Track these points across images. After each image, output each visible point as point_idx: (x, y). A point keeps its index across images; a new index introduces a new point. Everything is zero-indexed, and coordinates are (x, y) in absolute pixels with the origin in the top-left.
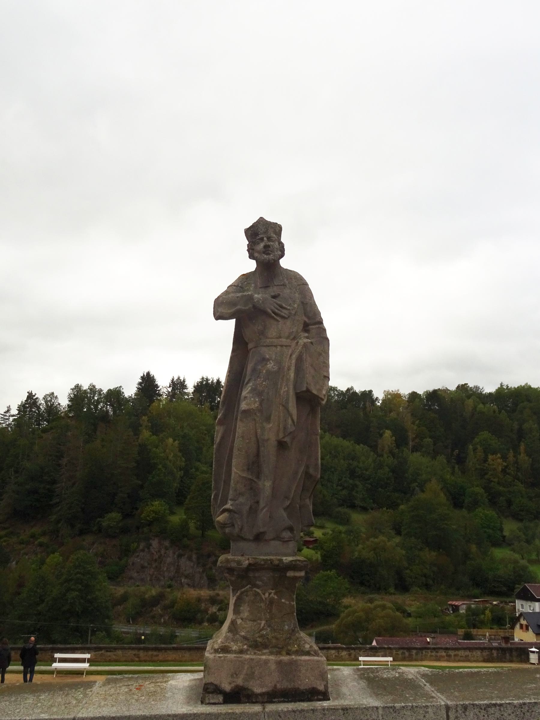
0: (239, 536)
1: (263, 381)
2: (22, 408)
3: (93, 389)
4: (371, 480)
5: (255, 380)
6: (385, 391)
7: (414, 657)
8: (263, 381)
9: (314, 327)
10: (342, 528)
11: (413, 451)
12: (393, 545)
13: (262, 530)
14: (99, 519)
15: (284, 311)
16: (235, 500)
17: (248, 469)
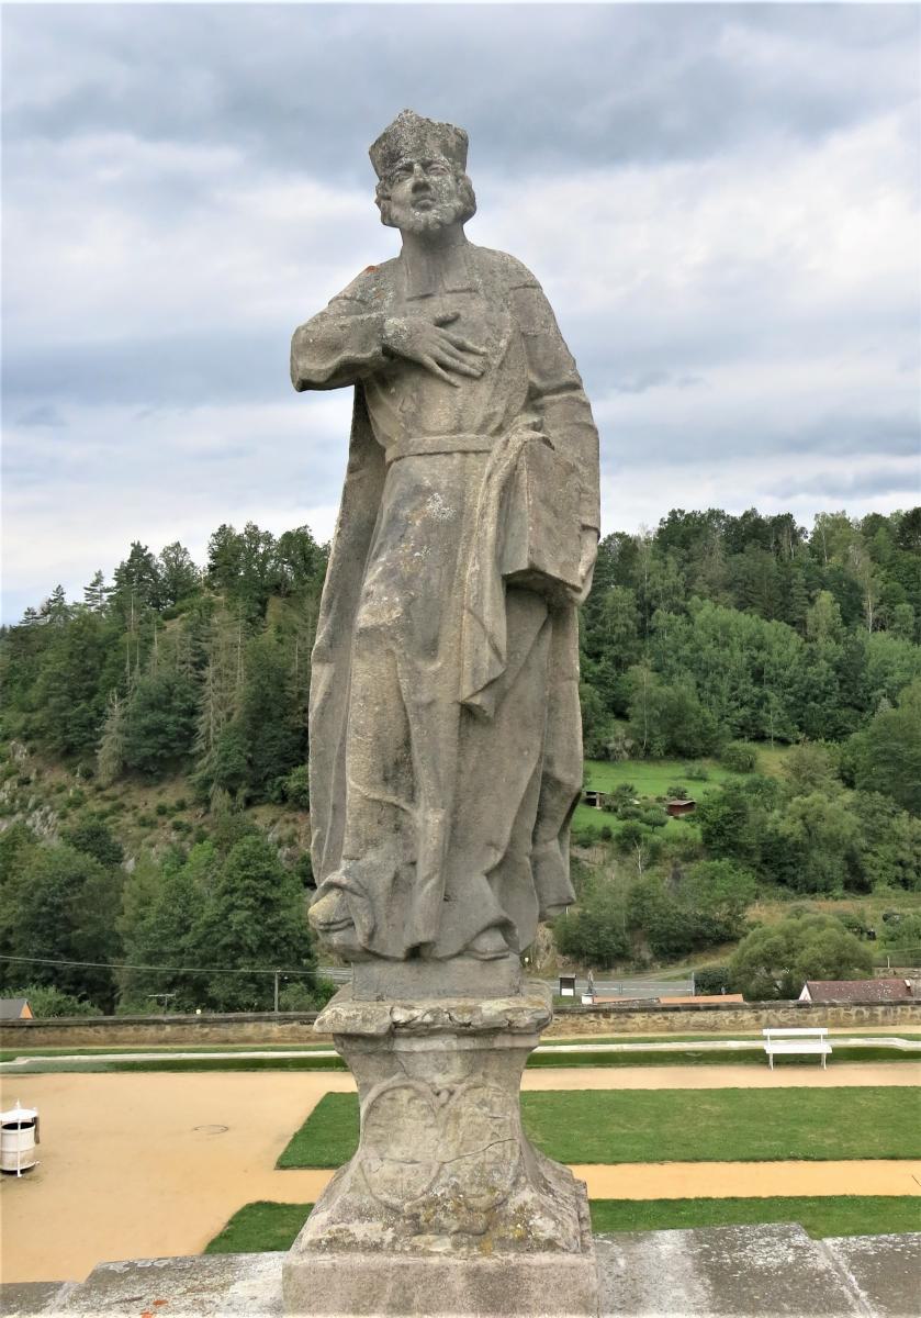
0: (367, 951)
1: (414, 550)
2: (125, 575)
3: (253, 534)
4: (796, 686)
5: (393, 547)
6: (817, 516)
7: (880, 1018)
8: (414, 550)
9: (556, 397)
10: (742, 780)
11: (875, 630)
12: (839, 808)
13: (422, 937)
14: (280, 778)
15: (472, 359)
16: (358, 859)
17: (386, 779)
